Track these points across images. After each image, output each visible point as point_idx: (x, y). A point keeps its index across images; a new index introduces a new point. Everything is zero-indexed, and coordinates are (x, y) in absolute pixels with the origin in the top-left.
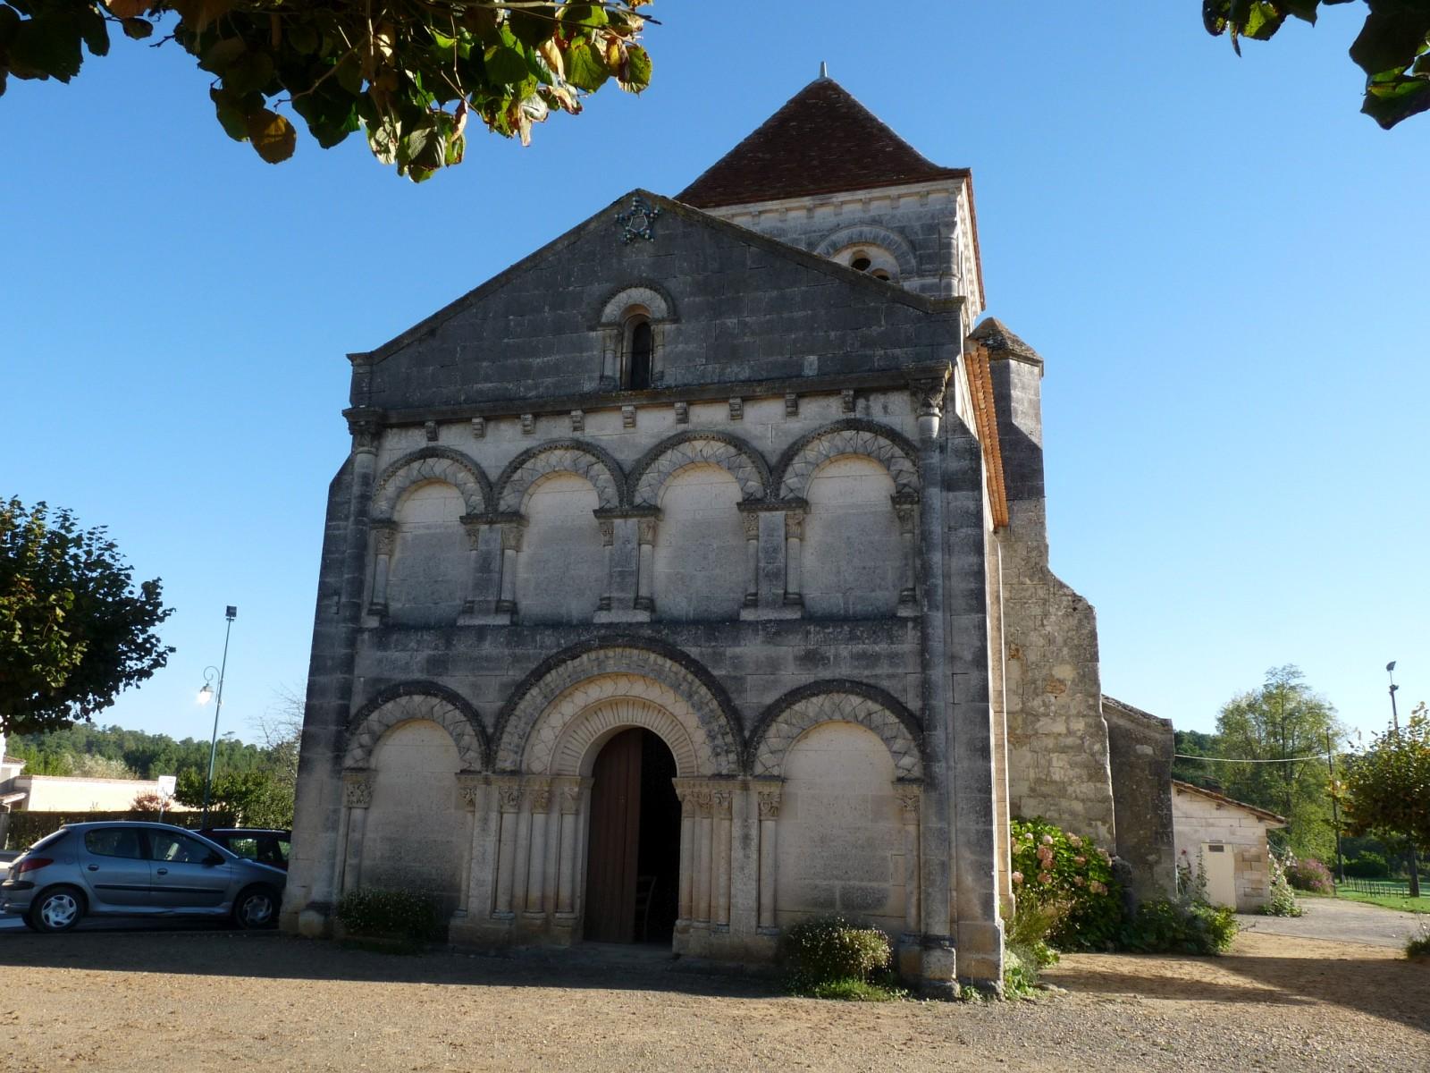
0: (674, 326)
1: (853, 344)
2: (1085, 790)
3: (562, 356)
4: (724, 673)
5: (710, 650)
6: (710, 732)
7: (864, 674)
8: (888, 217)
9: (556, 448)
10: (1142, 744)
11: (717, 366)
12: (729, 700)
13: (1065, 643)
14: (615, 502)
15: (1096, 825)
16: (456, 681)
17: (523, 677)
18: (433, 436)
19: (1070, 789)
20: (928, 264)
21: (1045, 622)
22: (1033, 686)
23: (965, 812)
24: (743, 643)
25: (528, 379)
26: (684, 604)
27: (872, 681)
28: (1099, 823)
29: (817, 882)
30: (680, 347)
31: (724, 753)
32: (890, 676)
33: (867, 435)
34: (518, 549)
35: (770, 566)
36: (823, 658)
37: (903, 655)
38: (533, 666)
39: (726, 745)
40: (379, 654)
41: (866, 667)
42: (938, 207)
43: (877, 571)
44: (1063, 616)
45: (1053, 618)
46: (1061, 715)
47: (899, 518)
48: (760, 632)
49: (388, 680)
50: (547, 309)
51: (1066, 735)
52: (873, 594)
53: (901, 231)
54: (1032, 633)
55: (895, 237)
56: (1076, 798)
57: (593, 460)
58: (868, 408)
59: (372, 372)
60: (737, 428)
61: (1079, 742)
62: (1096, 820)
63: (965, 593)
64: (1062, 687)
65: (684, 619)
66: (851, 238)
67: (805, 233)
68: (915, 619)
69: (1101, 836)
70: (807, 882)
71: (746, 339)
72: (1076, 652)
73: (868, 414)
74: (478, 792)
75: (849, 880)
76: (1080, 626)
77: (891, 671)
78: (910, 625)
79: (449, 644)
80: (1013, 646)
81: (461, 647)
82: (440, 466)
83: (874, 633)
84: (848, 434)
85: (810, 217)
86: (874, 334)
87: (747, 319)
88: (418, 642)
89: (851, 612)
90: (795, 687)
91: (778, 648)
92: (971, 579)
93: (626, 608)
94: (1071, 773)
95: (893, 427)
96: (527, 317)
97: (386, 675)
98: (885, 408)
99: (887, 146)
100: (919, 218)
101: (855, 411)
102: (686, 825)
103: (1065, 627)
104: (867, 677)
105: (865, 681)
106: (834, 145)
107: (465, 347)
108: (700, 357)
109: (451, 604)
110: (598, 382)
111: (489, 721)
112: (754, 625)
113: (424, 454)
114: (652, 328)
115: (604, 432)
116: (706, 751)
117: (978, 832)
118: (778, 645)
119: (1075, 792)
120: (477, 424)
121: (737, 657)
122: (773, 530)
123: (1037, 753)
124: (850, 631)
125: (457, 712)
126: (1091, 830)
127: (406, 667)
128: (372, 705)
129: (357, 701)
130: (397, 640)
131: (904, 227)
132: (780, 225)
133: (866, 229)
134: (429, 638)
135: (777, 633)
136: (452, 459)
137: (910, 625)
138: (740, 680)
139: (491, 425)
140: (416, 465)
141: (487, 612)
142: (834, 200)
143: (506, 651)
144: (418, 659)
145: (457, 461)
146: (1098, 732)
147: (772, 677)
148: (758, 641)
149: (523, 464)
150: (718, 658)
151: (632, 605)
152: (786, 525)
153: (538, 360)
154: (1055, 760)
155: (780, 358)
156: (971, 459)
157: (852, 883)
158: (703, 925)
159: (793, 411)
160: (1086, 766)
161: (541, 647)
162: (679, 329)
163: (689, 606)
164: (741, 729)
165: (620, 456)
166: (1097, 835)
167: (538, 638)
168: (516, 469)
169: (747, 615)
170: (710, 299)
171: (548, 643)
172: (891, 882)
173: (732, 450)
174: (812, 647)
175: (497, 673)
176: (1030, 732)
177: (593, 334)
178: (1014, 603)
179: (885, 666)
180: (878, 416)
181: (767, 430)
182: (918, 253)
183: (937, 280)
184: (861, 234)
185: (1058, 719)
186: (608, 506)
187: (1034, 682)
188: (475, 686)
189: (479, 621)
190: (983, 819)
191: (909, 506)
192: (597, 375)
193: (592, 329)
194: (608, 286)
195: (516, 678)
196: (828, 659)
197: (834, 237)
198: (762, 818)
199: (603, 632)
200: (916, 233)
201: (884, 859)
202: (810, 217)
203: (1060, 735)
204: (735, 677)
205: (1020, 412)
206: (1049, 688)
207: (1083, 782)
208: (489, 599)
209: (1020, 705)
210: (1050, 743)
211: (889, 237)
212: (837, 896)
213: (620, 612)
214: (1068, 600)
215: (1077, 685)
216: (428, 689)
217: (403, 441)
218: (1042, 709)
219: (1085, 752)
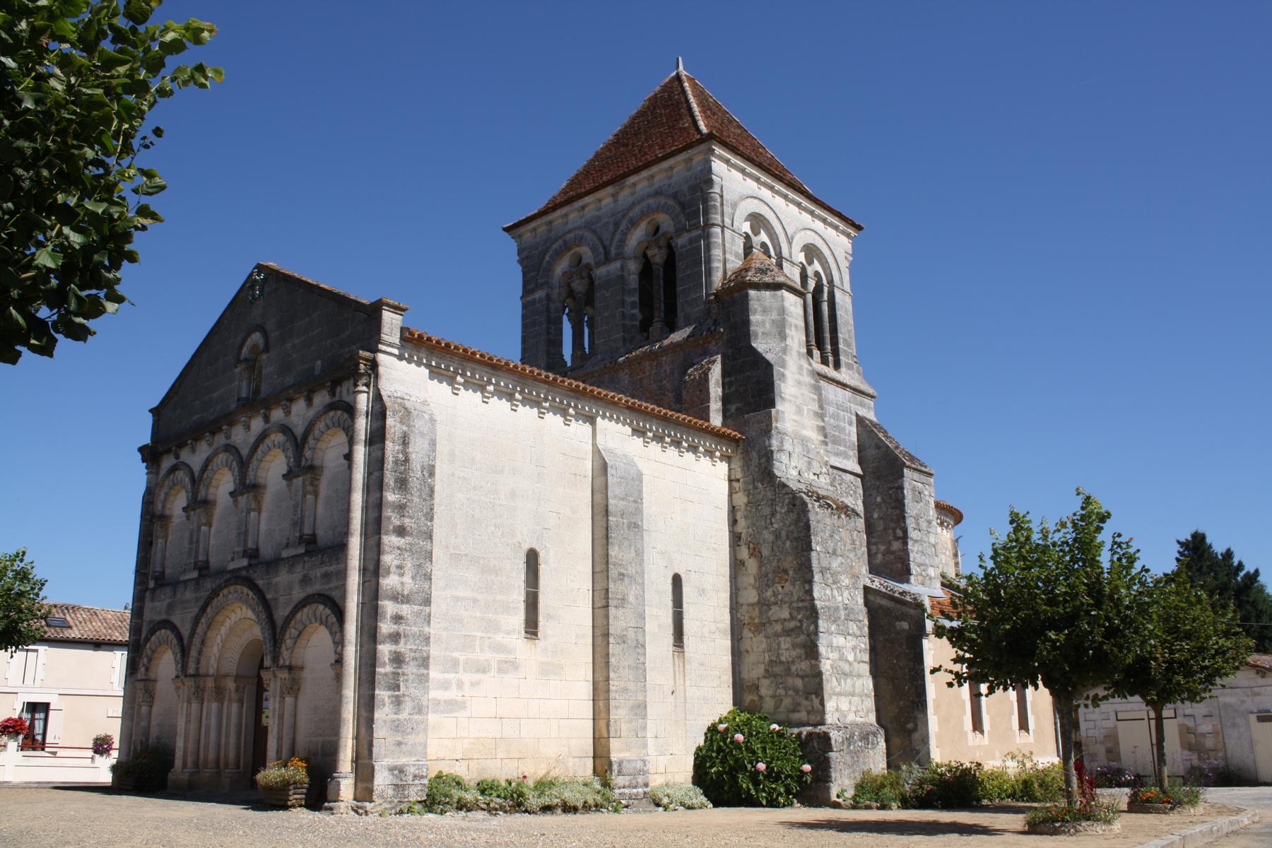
2: (804, 668)
10: (900, 621)
13: (788, 537)
19: (793, 668)
21: (773, 521)
28: (814, 696)
34: (209, 525)
42: (699, 168)
44: (785, 512)
45: (778, 516)
46: (786, 602)
51: (789, 620)
53: (675, 196)
55: (671, 202)
56: (798, 675)
61: (799, 624)
62: (812, 694)
64: (786, 577)
66: (642, 211)
72: (795, 544)
76: (798, 520)
85: (615, 201)
94: (794, 653)
103: (787, 523)
126: (808, 703)
132: (597, 213)
133: (651, 201)
142: (627, 183)
146: (812, 614)
154: (782, 643)
160: (804, 646)
166: (813, 707)
185: (784, 606)
192: (236, 398)
197: (631, 214)
202: (615, 201)
203: (785, 620)
207: (801, 661)
209: (757, 597)
210: (778, 628)
212: (320, 748)
219: (803, 633)
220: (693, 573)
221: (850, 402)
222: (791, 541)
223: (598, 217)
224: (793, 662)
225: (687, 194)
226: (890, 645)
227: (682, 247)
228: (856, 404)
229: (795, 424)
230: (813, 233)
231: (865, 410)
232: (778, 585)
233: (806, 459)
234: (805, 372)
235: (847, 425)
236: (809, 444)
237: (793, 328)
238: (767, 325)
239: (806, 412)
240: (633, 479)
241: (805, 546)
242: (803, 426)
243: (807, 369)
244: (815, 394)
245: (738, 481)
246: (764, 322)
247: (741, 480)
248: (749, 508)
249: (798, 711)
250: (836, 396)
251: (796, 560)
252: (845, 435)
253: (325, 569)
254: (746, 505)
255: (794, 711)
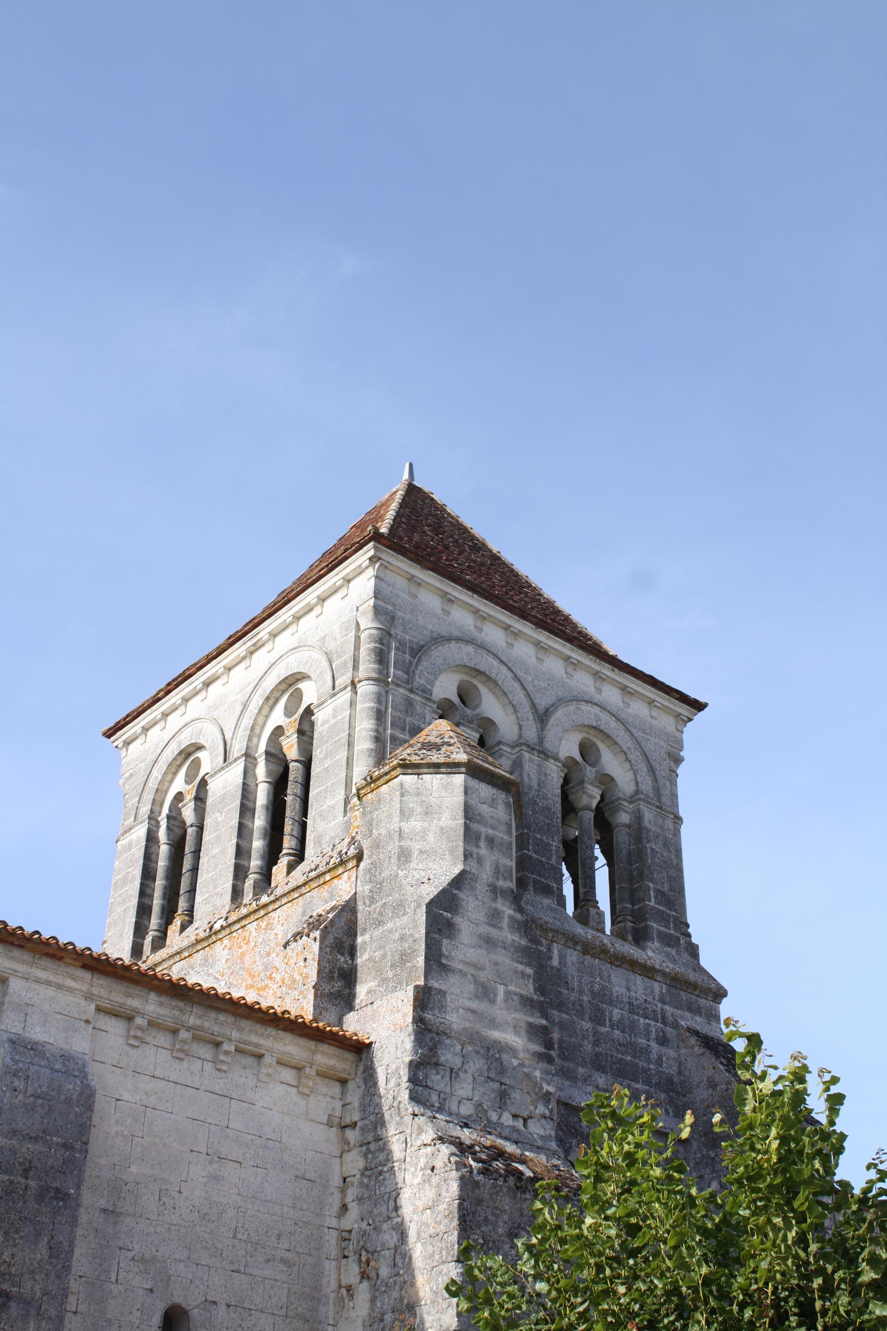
220: (222, 1309)
221: (662, 1001)
222: (424, 1244)
228: (679, 1007)
229: (471, 1017)
230: (596, 710)
231: (698, 1019)
233: (496, 1086)
234: (505, 923)
235: (653, 1044)
236: (505, 1057)
237: (482, 844)
238: (431, 838)
239: (501, 996)
240: (68, 1101)
242: (493, 1023)
243: (511, 918)
244: (528, 964)
245: (354, 1125)
248: (366, 1181)
250: (628, 989)
252: (649, 1061)
254: (362, 1174)
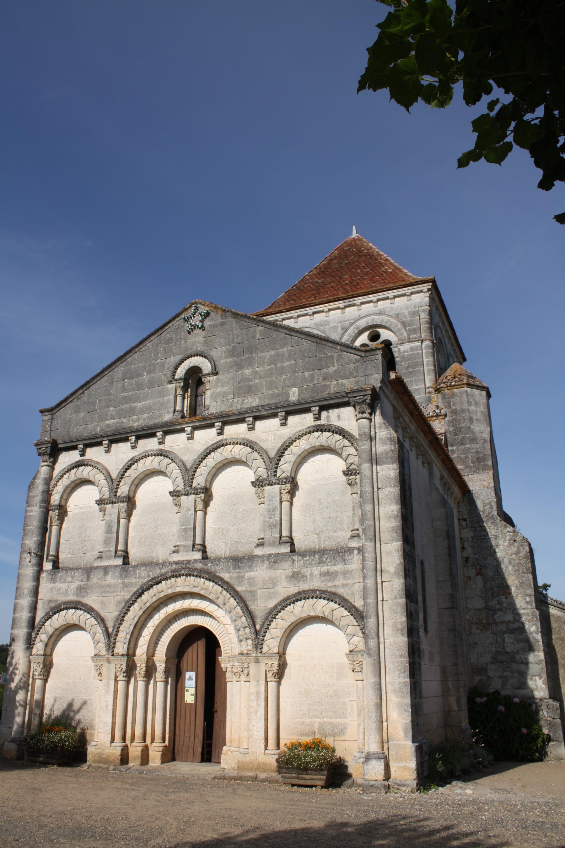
0: (215, 377)
1: (318, 379)
3: (153, 400)
4: (244, 588)
5: (235, 575)
6: (236, 626)
7: (328, 585)
8: (389, 309)
9: (148, 456)
11: (240, 399)
12: (246, 606)
13: (510, 563)
14: (181, 487)
15: (535, 679)
16: (90, 600)
17: (129, 596)
18: (83, 454)
19: (518, 657)
20: (413, 334)
22: (491, 592)
23: (391, 671)
24: (255, 569)
25: (134, 415)
26: (223, 547)
27: (333, 590)
28: (537, 678)
29: (304, 720)
30: (219, 389)
31: (244, 640)
32: (344, 586)
33: (328, 434)
35: (271, 520)
36: (303, 576)
37: (352, 571)
38: (135, 589)
39: (246, 634)
40: (52, 585)
41: (329, 581)
43: (338, 519)
47: (349, 484)
48: (266, 562)
49: (56, 600)
50: (145, 373)
52: (336, 534)
53: (397, 316)
54: (489, 558)
57: (170, 461)
58: (328, 417)
59: (52, 419)
60: (251, 436)
62: (535, 676)
63: (389, 529)
65: (223, 556)
67: (340, 322)
68: (359, 549)
69: (539, 686)
70: (298, 720)
71: (256, 381)
72: (517, 568)
73: (328, 421)
74: (104, 668)
75: (323, 718)
77: (344, 582)
78: (356, 552)
79: (88, 578)
80: (478, 567)
81: (95, 579)
82: (85, 472)
83: (334, 558)
84: (316, 434)
86: (331, 372)
87: (257, 369)
88: (72, 577)
89: (322, 546)
90: (286, 596)
91: (276, 571)
92: (393, 520)
93: (187, 551)
95: (344, 427)
96: (134, 380)
97: (55, 597)
98: (339, 416)
99: (389, 269)
100: (407, 308)
101: (320, 420)
102: (229, 685)
104: (330, 587)
105: (329, 589)
106: (359, 271)
107: (101, 400)
108: (230, 394)
109: (92, 553)
110: (172, 414)
111: (110, 625)
112: (263, 558)
113: (78, 465)
114: (203, 379)
115: (176, 444)
116: (235, 640)
117: (400, 683)
118: (277, 570)
119: (521, 658)
120: (105, 444)
121: (251, 579)
122: (273, 497)
123: (496, 634)
124: (319, 559)
125: (93, 619)
127: (66, 593)
128: (48, 617)
129: (40, 614)
130: (61, 577)
131: (398, 314)
134: (78, 575)
135: (275, 562)
136: (92, 466)
137: (356, 552)
138: (253, 593)
139: (114, 446)
140: (73, 471)
141: (109, 558)
143: (120, 581)
144: (72, 587)
145: (95, 467)
147: (273, 590)
148: (264, 568)
149: (131, 466)
150: (240, 579)
151: (191, 548)
152: (281, 493)
153: (140, 404)
155: (276, 391)
156: (391, 444)
157: (325, 720)
158: (236, 749)
159: (284, 424)
161: (139, 577)
162: (218, 379)
163: (226, 548)
164: (254, 625)
165: (184, 458)
167: (138, 572)
168: (127, 469)
169: (259, 552)
170: (236, 359)
171: (143, 574)
172: (349, 718)
173: (249, 450)
174: (296, 570)
175: (114, 594)
176: (491, 622)
177: (170, 386)
178: (477, 540)
179: (341, 580)
180: (335, 422)
181: (269, 435)
182: (407, 328)
183: (420, 344)
184: (382, 321)
186: (177, 489)
187: (492, 589)
188: (103, 603)
189: (105, 563)
190: (403, 675)
191: (354, 476)
193: (170, 382)
194: (179, 358)
195: (125, 597)
196: (306, 577)
198: (268, 680)
199: (174, 566)
200: (406, 317)
201: (344, 703)
203: (509, 622)
204: (251, 592)
205: (475, 420)
206: (501, 592)
208: (111, 549)
210: (504, 627)
211: (390, 320)
213: (185, 554)
214: (510, 536)
215: (519, 589)
216: (76, 605)
217: (67, 458)
218: (498, 606)
223: (328, 322)
224: (517, 652)
225: (408, 316)
226: (561, 642)
227: (404, 352)
232: (502, 596)
238: (478, 414)
241: (525, 570)
246: (476, 411)
247: (468, 520)
249: (524, 689)
251: (517, 579)
253: (324, 569)
255: (519, 688)
